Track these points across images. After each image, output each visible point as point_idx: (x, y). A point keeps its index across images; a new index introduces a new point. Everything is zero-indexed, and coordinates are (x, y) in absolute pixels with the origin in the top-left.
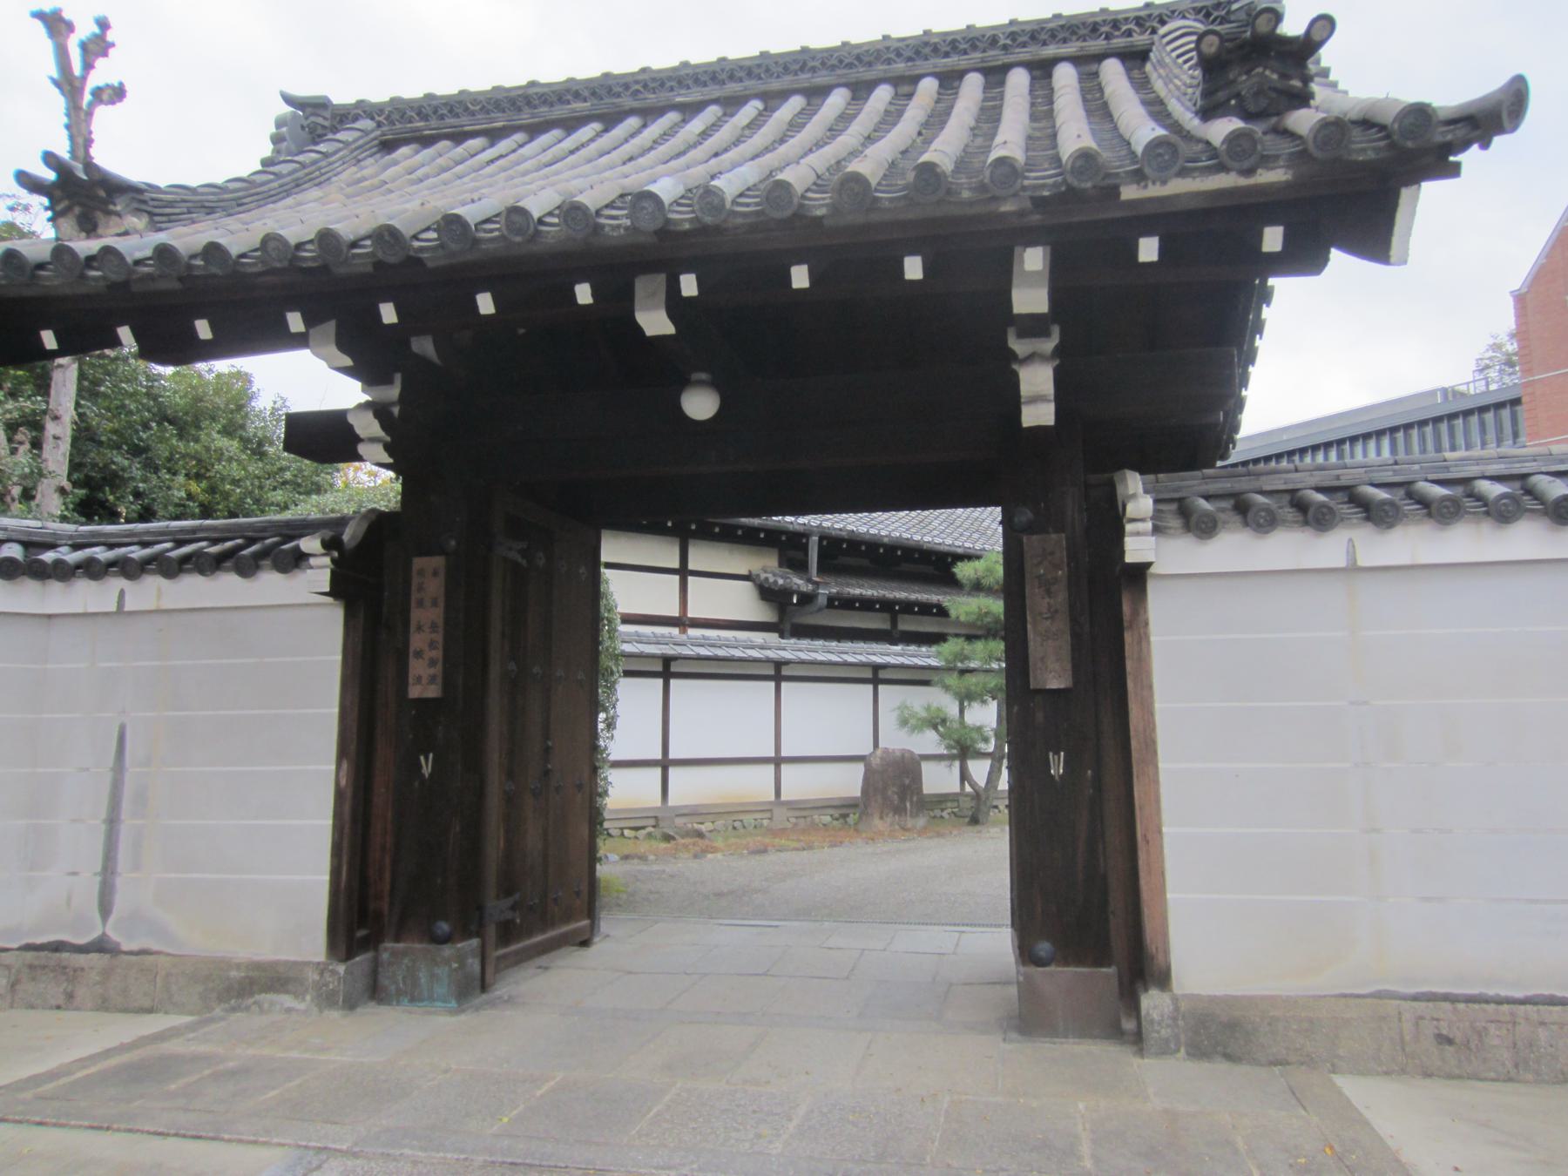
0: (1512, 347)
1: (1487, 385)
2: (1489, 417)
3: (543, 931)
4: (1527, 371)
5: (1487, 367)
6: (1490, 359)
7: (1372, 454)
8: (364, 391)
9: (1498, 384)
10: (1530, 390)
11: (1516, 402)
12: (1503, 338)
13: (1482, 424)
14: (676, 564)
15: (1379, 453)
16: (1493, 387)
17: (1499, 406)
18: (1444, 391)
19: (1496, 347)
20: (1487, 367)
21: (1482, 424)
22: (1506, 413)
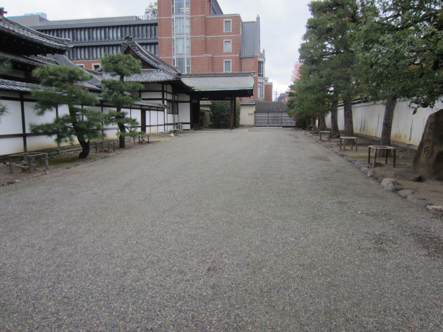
0: (156, 8)
1: (148, 18)
2: (149, 28)
3: (217, 35)
4: (159, 15)
5: (148, 12)
6: (149, 10)
7: (115, 52)
8: (312, 14)
9: (152, 18)
10: (160, 21)
11: (156, 24)
12: (153, 4)
13: (138, 29)
14: (161, 97)
15: (113, 53)
16: (149, 19)
17: (151, 25)
18: (136, 17)
19: (151, 6)
20: (148, 12)
21: (138, 29)
22: (153, 28)
